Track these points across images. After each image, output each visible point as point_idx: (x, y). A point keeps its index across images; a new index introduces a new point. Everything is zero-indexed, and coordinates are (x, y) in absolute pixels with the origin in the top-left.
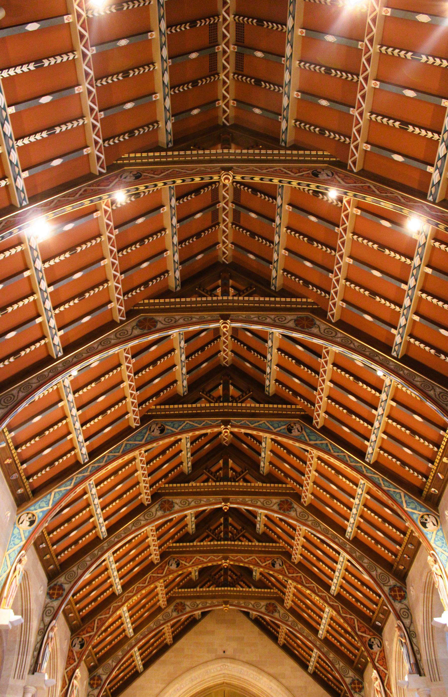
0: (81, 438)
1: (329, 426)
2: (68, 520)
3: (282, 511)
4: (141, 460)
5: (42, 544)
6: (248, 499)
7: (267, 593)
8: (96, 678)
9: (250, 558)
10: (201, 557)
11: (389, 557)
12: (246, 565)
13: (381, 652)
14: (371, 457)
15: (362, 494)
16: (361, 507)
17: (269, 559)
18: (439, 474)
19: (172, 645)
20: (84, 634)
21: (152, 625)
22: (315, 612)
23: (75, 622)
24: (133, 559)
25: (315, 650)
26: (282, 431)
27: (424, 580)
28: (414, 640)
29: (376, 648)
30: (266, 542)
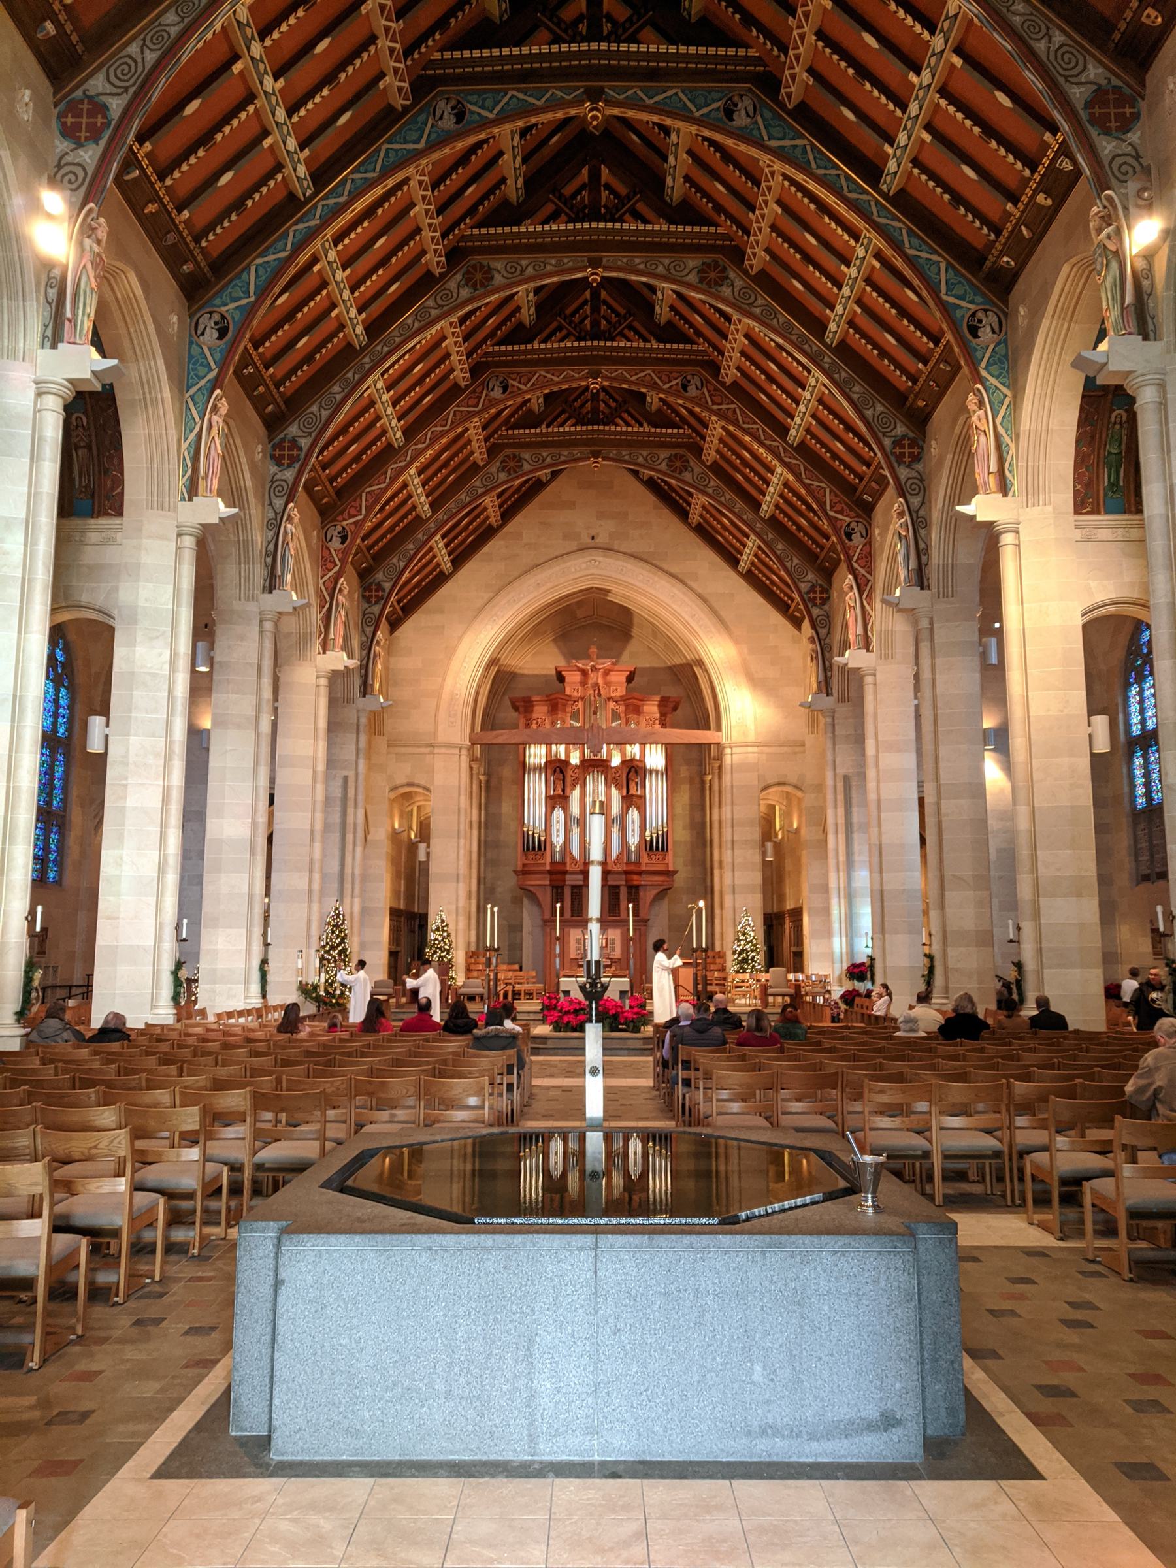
0: (292, 143)
1: (815, 105)
2: (289, 317)
3: (704, 286)
4: (420, 182)
5: (246, 367)
6: (638, 260)
7: (672, 435)
8: (374, 587)
9: (642, 374)
10: (548, 372)
11: (902, 382)
12: (634, 388)
13: (865, 545)
14: (891, 183)
15: (864, 258)
16: (860, 283)
17: (675, 375)
18: (1023, 228)
19: (500, 527)
20: (345, 520)
21: (463, 497)
22: (757, 473)
23: (325, 500)
24: (420, 381)
25: (753, 537)
26: (713, 115)
27: (957, 430)
28: (923, 532)
29: (857, 538)
30: (672, 342)
